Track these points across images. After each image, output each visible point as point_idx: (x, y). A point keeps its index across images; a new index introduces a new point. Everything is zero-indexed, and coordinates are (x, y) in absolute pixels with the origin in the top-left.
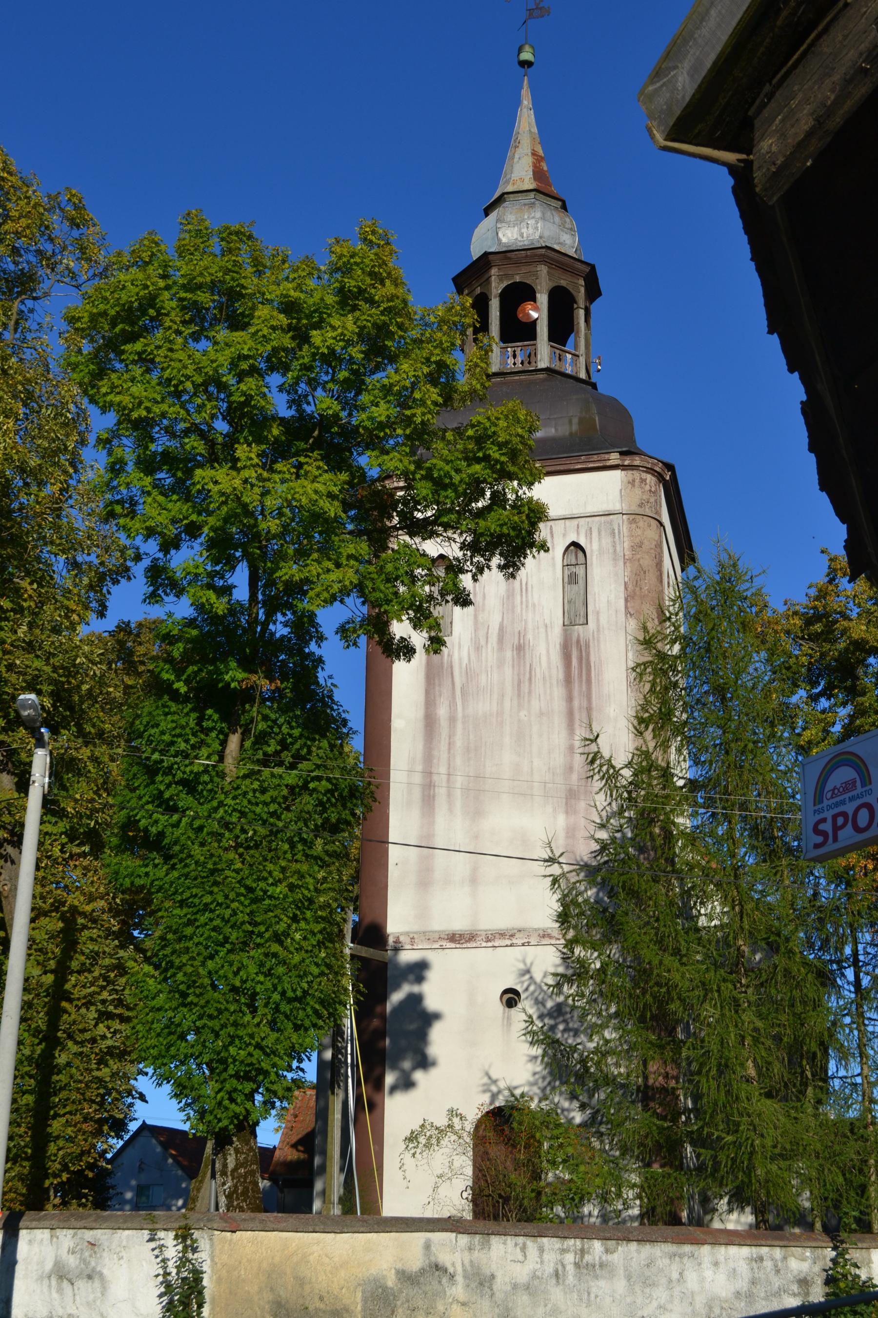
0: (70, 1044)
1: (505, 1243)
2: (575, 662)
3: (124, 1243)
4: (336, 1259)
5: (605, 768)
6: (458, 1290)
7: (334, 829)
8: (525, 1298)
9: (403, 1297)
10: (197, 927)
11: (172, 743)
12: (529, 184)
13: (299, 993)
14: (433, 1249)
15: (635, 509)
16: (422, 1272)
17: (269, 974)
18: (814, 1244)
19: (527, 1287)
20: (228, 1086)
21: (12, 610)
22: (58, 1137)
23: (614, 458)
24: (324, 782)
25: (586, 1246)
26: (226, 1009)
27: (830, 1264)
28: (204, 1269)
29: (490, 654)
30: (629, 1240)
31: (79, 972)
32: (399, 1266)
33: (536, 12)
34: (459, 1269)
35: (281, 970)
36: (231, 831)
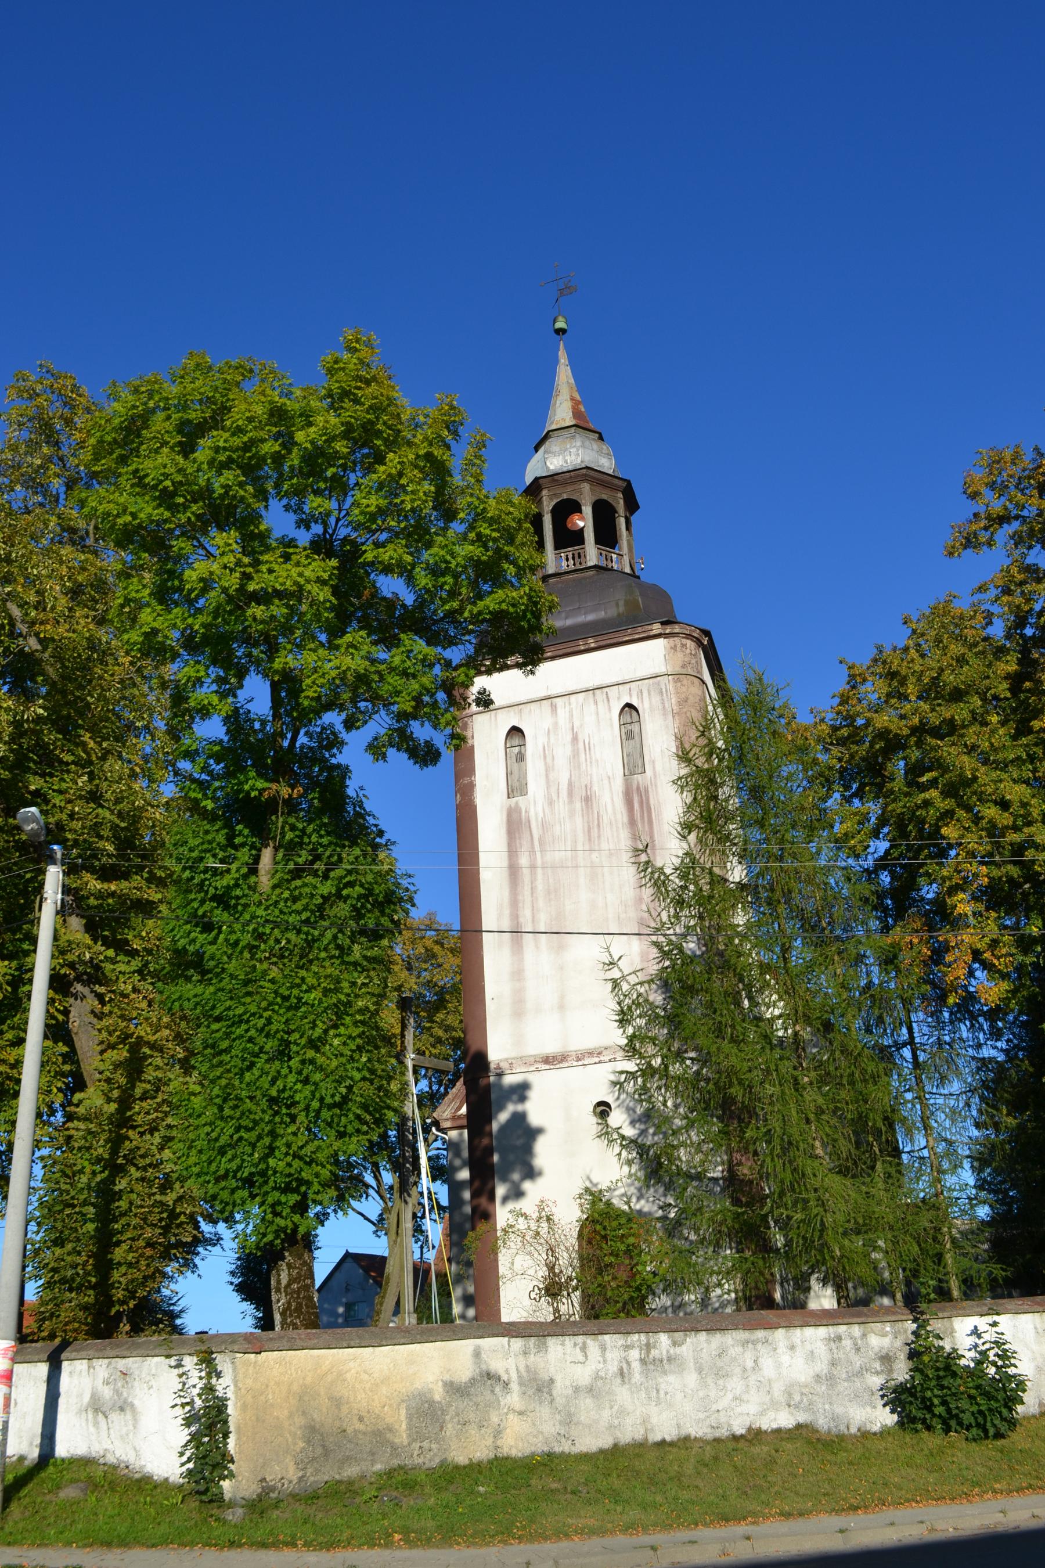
0: (133, 1170)
1: (563, 1344)
2: (636, 806)
3: (153, 1372)
4: (375, 1375)
5: (656, 875)
6: (514, 1399)
7: (375, 936)
8: (589, 1401)
9: (452, 1411)
10: (234, 1040)
11: (201, 859)
12: (569, 421)
13: (337, 1098)
14: (484, 1356)
15: (678, 670)
16: (473, 1382)
17: (306, 1081)
18: (893, 1318)
19: (590, 1390)
20: (270, 1200)
21: (73, 762)
22: (119, 1264)
23: (657, 628)
24: (357, 888)
25: (652, 1341)
26: (261, 1119)
27: (913, 1338)
28: (228, 1396)
29: (562, 807)
30: (698, 1331)
31: (141, 1099)
32: (447, 1377)
33: (565, 291)
34: (514, 1376)
35: (317, 1077)
36: (265, 942)
